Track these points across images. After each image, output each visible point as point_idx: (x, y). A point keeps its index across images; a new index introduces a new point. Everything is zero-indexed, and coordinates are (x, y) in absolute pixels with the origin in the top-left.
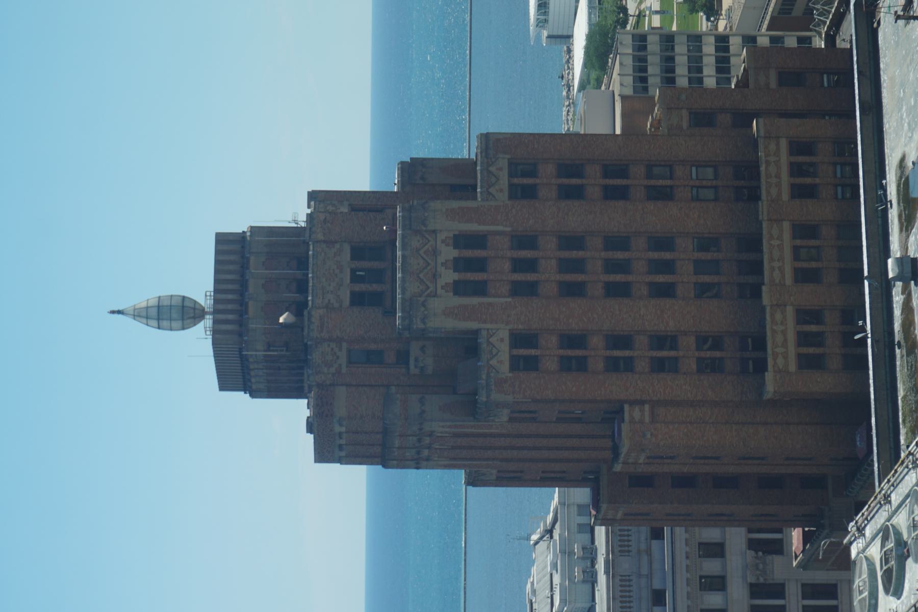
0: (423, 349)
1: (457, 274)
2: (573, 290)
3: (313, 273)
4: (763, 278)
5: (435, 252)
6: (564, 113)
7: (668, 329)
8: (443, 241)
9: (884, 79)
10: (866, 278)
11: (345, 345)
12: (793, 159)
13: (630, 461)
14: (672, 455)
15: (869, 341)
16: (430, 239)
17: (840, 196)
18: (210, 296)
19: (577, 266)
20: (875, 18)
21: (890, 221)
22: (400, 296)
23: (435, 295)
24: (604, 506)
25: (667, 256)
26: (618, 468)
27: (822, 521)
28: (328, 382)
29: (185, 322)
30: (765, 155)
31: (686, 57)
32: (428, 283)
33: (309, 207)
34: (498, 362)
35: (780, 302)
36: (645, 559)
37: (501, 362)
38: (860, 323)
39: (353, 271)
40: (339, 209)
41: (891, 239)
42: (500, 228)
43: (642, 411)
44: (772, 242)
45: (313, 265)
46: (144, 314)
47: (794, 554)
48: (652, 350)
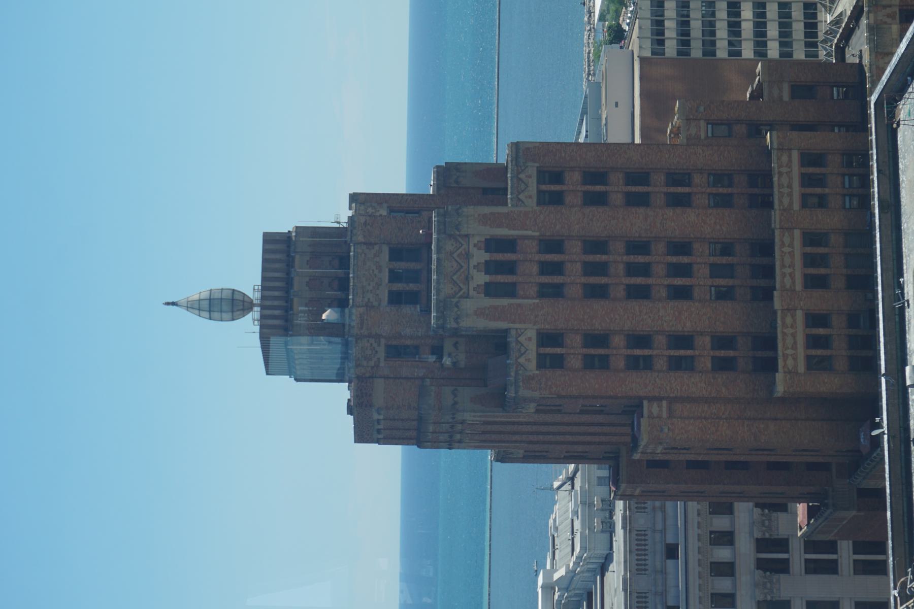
0: (455, 345)
1: (488, 276)
2: (597, 292)
3: (354, 273)
4: (775, 282)
5: (467, 256)
6: (586, 37)
7: (685, 329)
8: (475, 245)
9: (903, 180)
10: (883, 375)
11: (383, 341)
12: (804, 170)
13: (649, 451)
14: (687, 447)
15: (886, 437)
16: (463, 242)
17: (847, 206)
18: (258, 290)
19: (601, 269)
20: (894, 118)
21: (907, 319)
22: (435, 297)
23: (467, 297)
24: (623, 486)
25: (685, 260)
26: (637, 456)
27: (826, 501)
28: (367, 375)
29: (235, 314)
30: (778, 166)
31: (700, 22)
32: (461, 285)
33: (350, 209)
34: (526, 360)
35: (790, 306)
36: (659, 515)
37: (529, 360)
38: (878, 420)
39: (391, 272)
40: (379, 211)
41: (907, 336)
42: (529, 233)
43: (660, 407)
44: (784, 249)
45: (354, 265)
46: (196, 306)
47: (799, 525)
48: (670, 349)
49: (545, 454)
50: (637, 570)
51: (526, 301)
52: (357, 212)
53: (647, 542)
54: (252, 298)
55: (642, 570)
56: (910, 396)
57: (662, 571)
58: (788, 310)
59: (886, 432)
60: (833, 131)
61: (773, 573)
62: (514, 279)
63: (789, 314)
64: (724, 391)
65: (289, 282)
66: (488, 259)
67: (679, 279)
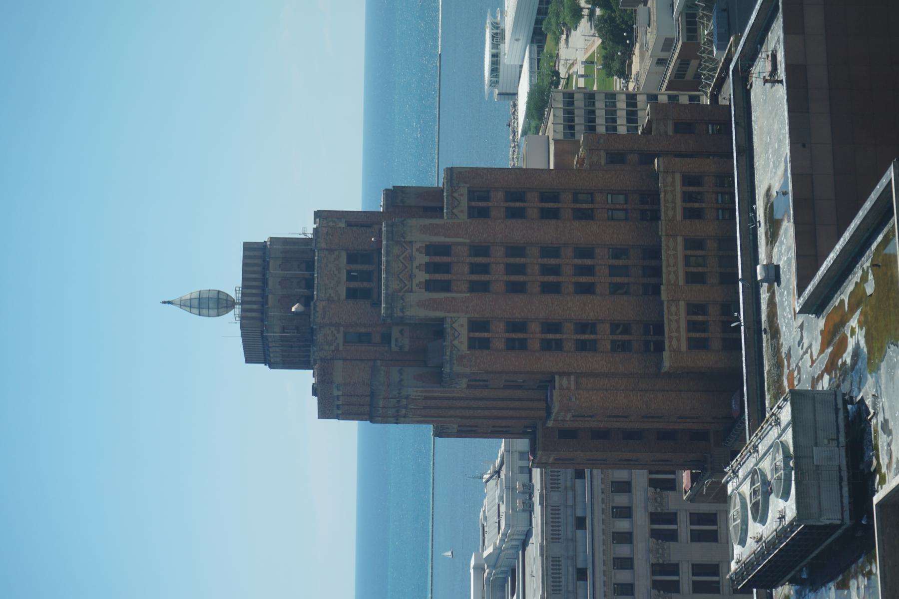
0: (401, 332)
1: (428, 275)
2: (517, 288)
5: (411, 258)
6: (511, 153)
8: (417, 250)
9: (755, 129)
10: (741, 280)
11: (342, 329)
13: (560, 418)
16: (407, 248)
17: (721, 217)
18: (239, 290)
21: (759, 237)
22: (384, 292)
23: (411, 291)
25: (588, 262)
26: (550, 424)
28: (329, 358)
31: (604, 111)
32: (406, 282)
33: (315, 223)
34: (459, 342)
36: (570, 494)
37: (461, 342)
38: (736, 314)
39: (348, 272)
41: (759, 250)
42: (461, 240)
46: (188, 304)
47: (684, 491)
49: (474, 428)
50: (553, 590)
51: (459, 295)
52: (321, 225)
53: (560, 516)
54: (234, 298)
55: (556, 539)
56: (761, 296)
57: (572, 540)
58: (673, 300)
59: (743, 324)
60: (709, 158)
61: (664, 541)
62: (450, 277)
63: (673, 304)
64: (621, 367)
65: (265, 281)
66: (428, 261)
67: (584, 277)
